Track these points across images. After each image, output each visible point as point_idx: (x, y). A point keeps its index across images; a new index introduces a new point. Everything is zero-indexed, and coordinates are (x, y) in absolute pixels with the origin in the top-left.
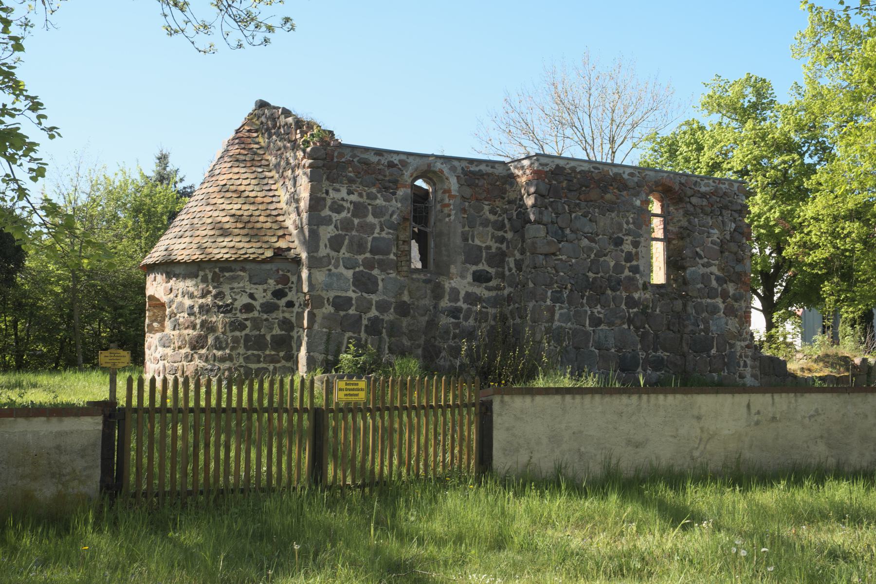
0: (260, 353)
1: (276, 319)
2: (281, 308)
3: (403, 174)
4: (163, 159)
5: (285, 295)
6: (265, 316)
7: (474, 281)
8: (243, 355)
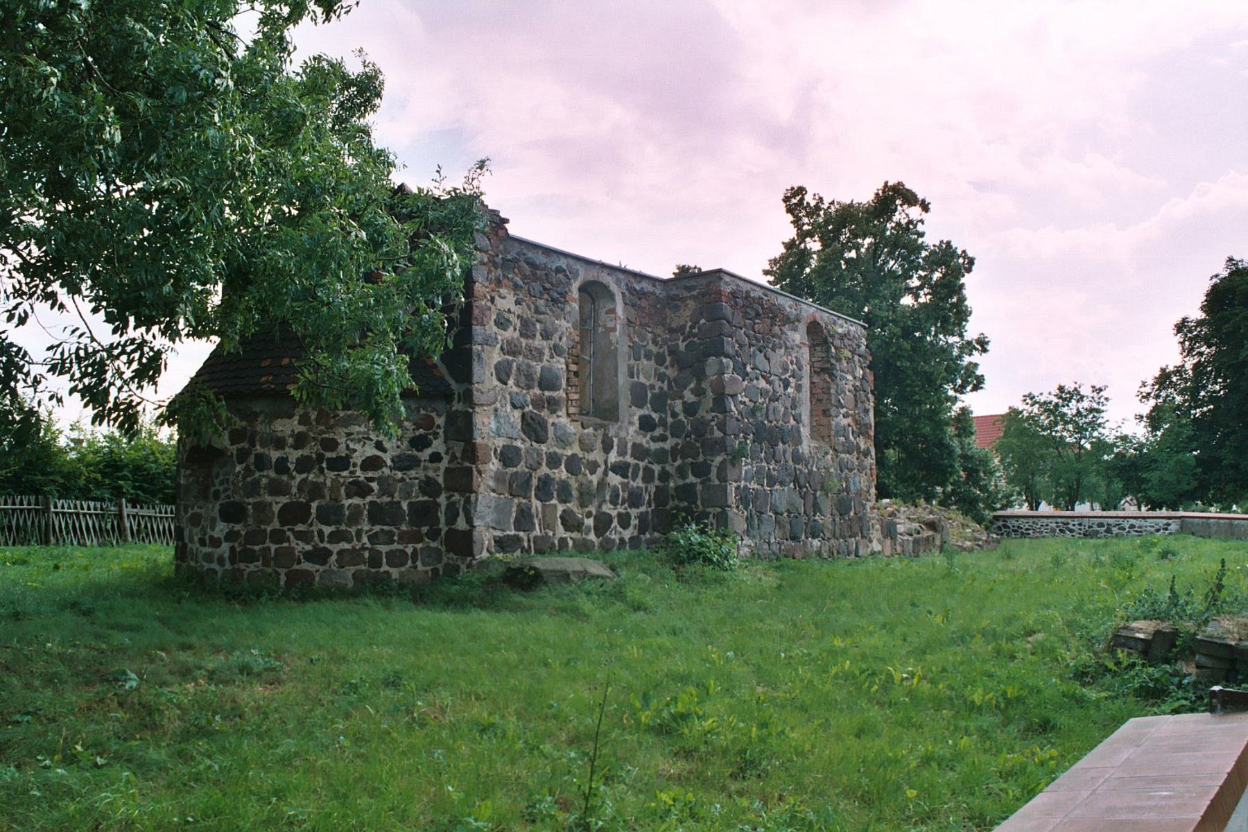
0: (392, 528)
1: (416, 478)
2: (422, 464)
3: (571, 284)
4: (969, 183)
5: (429, 444)
6: (399, 475)
7: (640, 429)
8: (367, 532)
